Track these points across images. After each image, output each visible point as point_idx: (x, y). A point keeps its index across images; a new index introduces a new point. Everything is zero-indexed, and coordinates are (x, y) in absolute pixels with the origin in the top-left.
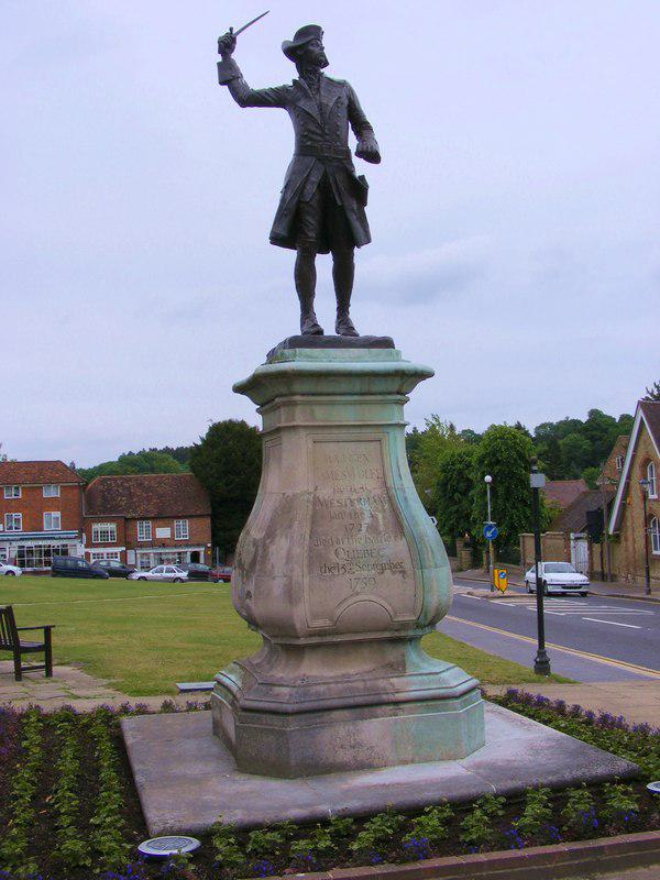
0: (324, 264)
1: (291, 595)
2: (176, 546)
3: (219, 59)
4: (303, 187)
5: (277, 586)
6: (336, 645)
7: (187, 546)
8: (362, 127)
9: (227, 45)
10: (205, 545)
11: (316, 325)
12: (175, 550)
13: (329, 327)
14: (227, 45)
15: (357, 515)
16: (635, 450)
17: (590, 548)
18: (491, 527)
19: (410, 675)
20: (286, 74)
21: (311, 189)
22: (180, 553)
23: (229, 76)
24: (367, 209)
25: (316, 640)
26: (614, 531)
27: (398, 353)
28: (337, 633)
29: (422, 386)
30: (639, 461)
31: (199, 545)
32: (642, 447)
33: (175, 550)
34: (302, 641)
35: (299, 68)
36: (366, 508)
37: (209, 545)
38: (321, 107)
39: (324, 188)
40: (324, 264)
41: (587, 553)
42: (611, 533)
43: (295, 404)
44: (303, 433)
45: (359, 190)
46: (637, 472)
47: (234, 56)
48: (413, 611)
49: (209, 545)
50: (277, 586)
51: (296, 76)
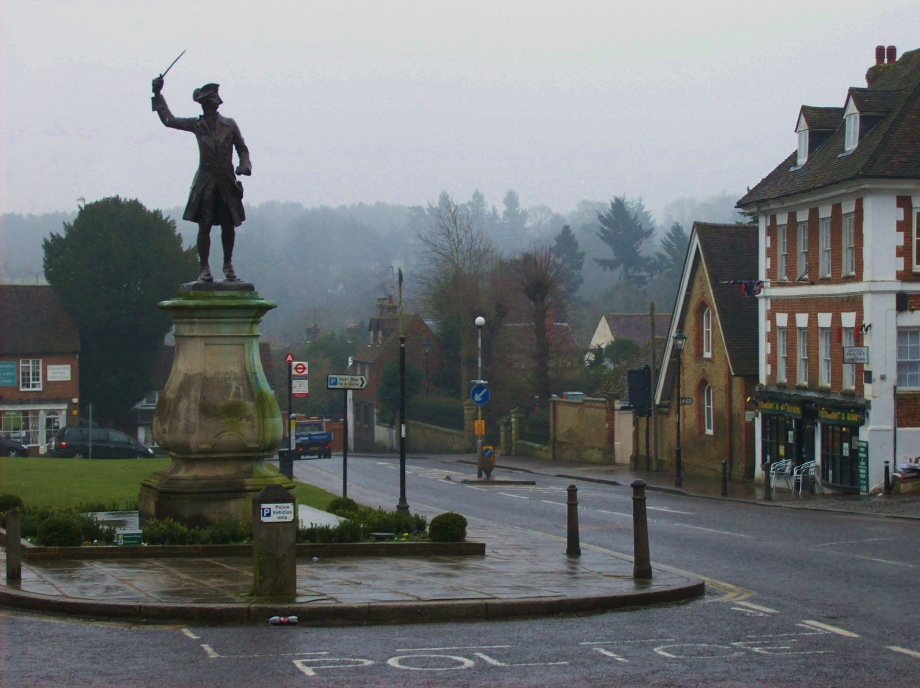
0: (216, 232)
1: (188, 430)
2: (21, 402)
3: (153, 95)
4: (203, 191)
5: (181, 425)
6: (216, 459)
7: (39, 401)
8: (243, 151)
9: (158, 84)
10: (68, 401)
11: (209, 275)
12: (20, 408)
13: (219, 277)
14: (158, 84)
15: (229, 387)
16: (689, 289)
17: (636, 423)
18: (481, 387)
19: (256, 478)
20: (196, 111)
21: (208, 193)
22: (26, 413)
23: (159, 104)
24: (244, 201)
25: (201, 456)
26: (662, 399)
27: (256, 293)
28: (215, 452)
29: (269, 313)
30: (693, 304)
31: (58, 401)
32: (697, 284)
33: (20, 408)
34: (193, 456)
35: (204, 108)
36: (234, 384)
37: (75, 400)
38: (215, 142)
39: (217, 192)
40: (216, 232)
41: (632, 429)
42: (658, 402)
43: (194, 323)
44: (198, 341)
45: (238, 191)
46: (691, 319)
47: (162, 92)
48: (257, 442)
49: (75, 400)
50: (181, 425)
51: (202, 113)
